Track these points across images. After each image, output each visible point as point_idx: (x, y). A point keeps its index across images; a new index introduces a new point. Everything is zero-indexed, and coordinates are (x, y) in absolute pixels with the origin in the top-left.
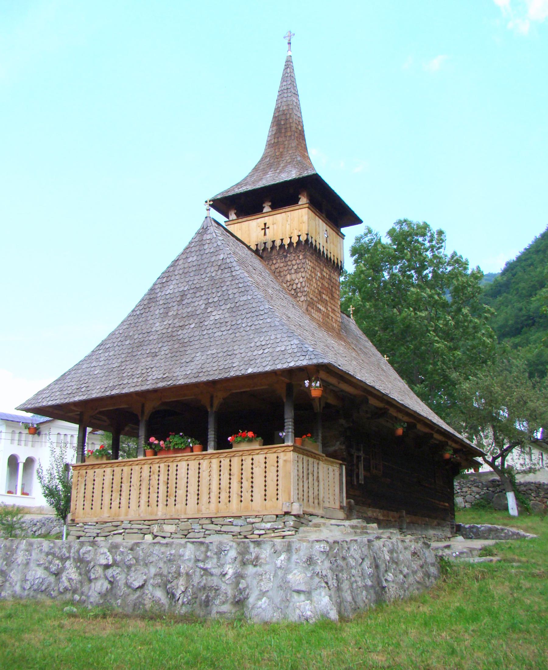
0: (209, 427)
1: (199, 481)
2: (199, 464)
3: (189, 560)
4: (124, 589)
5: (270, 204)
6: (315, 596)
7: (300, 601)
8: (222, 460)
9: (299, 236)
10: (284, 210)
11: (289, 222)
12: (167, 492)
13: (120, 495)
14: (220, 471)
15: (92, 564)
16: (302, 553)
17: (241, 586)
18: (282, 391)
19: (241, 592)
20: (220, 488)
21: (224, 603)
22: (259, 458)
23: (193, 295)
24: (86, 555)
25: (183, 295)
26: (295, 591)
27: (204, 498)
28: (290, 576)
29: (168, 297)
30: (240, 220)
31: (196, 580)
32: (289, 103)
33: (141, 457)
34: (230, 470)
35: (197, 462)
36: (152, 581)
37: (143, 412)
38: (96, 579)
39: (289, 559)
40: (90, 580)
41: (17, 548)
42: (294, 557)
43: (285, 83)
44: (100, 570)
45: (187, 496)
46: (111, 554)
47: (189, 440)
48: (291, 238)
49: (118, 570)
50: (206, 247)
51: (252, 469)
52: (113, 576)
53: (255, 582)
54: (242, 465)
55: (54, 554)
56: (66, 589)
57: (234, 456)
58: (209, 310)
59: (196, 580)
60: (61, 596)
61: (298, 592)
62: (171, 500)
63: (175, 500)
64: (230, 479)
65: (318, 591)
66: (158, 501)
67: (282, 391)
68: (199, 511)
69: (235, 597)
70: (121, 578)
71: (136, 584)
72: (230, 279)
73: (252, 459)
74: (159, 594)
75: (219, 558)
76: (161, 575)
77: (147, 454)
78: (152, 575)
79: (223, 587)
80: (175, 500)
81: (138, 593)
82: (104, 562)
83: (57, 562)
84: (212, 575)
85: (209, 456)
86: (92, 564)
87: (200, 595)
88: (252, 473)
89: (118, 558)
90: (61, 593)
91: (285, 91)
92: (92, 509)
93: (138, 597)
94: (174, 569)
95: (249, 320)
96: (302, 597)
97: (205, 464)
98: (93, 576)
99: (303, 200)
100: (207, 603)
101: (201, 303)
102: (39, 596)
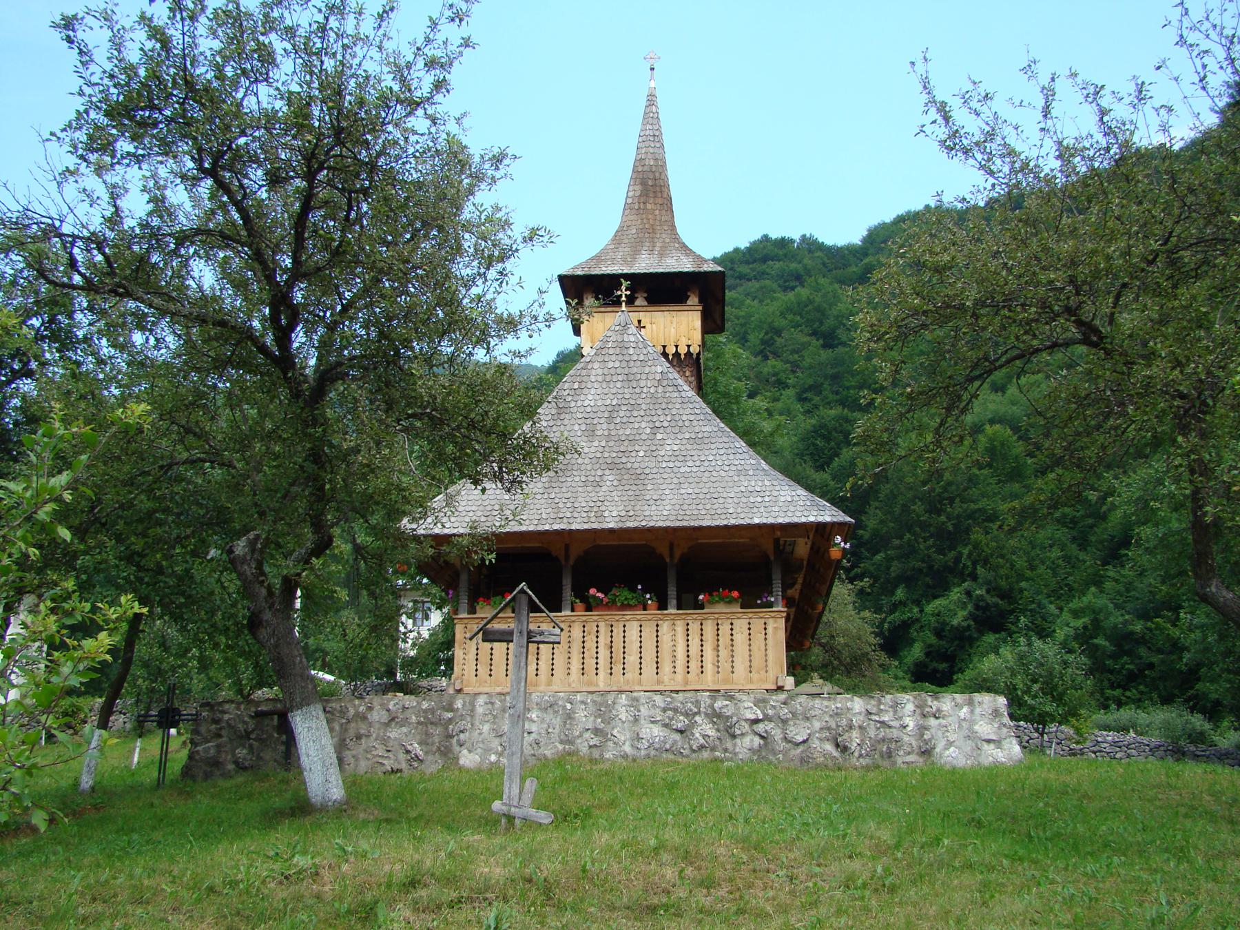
0: (564, 582)
1: (657, 647)
2: (657, 626)
3: (860, 713)
4: (782, 745)
5: (646, 295)
6: (1006, 744)
7: (989, 749)
8: (690, 622)
9: (689, 346)
10: (668, 308)
11: (674, 325)
12: (611, 658)
13: (537, 659)
14: (688, 635)
15: (735, 719)
16: (985, 706)
17: (925, 737)
18: (769, 548)
19: (926, 742)
20: (688, 656)
21: (909, 753)
22: (741, 624)
23: (628, 414)
24: (723, 710)
25: (613, 410)
26: (984, 740)
27: (666, 668)
28: (976, 727)
29: (589, 409)
30: (603, 309)
31: (872, 733)
32: (657, 156)
33: (568, 613)
34: (702, 635)
35: (639, 623)
36: (817, 735)
37: (567, 557)
38: (742, 734)
39: (972, 712)
40: (734, 736)
41: (614, 703)
42: (978, 710)
43: (648, 127)
44: (746, 727)
45: (641, 663)
46: (758, 707)
47: (648, 596)
48: (677, 346)
49: (771, 725)
50: (631, 351)
51: (732, 635)
52: (766, 732)
53: (940, 734)
54: (718, 630)
55: (675, 710)
56: (702, 747)
57: (706, 619)
58: (659, 436)
59: (872, 733)
60: (694, 755)
61: (989, 741)
62: (618, 668)
63: (624, 669)
64: (702, 645)
65: (1008, 740)
66: (597, 669)
67: (769, 548)
68: (659, 682)
69: (920, 747)
70: (777, 734)
71: (799, 739)
72: (680, 400)
73: (732, 624)
74: (829, 747)
75: (895, 712)
76: (829, 729)
77: (576, 609)
78: (818, 729)
79: (906, 738)
80: (624, 669)
81: (801, 748)
82: (753, 717)
83: (681, 718)
84: (890, 727)
85: (672, 617)
86: (735, 719)
87: (879, 747)
88: (732, 640)
89: (770, 712)
90: (694, 751)
91: (652, 139)
92: (490, 675)
93: (802, 752)
94: (844, 722)
95: (724, 458)
96: (992, 746)
97: (665, 627)
98: (738, 732)
99: (693, 300)
100: (890, 755)
101: (643, 425)
102: (664, 755)
